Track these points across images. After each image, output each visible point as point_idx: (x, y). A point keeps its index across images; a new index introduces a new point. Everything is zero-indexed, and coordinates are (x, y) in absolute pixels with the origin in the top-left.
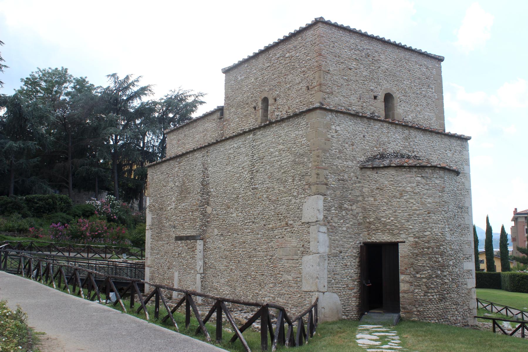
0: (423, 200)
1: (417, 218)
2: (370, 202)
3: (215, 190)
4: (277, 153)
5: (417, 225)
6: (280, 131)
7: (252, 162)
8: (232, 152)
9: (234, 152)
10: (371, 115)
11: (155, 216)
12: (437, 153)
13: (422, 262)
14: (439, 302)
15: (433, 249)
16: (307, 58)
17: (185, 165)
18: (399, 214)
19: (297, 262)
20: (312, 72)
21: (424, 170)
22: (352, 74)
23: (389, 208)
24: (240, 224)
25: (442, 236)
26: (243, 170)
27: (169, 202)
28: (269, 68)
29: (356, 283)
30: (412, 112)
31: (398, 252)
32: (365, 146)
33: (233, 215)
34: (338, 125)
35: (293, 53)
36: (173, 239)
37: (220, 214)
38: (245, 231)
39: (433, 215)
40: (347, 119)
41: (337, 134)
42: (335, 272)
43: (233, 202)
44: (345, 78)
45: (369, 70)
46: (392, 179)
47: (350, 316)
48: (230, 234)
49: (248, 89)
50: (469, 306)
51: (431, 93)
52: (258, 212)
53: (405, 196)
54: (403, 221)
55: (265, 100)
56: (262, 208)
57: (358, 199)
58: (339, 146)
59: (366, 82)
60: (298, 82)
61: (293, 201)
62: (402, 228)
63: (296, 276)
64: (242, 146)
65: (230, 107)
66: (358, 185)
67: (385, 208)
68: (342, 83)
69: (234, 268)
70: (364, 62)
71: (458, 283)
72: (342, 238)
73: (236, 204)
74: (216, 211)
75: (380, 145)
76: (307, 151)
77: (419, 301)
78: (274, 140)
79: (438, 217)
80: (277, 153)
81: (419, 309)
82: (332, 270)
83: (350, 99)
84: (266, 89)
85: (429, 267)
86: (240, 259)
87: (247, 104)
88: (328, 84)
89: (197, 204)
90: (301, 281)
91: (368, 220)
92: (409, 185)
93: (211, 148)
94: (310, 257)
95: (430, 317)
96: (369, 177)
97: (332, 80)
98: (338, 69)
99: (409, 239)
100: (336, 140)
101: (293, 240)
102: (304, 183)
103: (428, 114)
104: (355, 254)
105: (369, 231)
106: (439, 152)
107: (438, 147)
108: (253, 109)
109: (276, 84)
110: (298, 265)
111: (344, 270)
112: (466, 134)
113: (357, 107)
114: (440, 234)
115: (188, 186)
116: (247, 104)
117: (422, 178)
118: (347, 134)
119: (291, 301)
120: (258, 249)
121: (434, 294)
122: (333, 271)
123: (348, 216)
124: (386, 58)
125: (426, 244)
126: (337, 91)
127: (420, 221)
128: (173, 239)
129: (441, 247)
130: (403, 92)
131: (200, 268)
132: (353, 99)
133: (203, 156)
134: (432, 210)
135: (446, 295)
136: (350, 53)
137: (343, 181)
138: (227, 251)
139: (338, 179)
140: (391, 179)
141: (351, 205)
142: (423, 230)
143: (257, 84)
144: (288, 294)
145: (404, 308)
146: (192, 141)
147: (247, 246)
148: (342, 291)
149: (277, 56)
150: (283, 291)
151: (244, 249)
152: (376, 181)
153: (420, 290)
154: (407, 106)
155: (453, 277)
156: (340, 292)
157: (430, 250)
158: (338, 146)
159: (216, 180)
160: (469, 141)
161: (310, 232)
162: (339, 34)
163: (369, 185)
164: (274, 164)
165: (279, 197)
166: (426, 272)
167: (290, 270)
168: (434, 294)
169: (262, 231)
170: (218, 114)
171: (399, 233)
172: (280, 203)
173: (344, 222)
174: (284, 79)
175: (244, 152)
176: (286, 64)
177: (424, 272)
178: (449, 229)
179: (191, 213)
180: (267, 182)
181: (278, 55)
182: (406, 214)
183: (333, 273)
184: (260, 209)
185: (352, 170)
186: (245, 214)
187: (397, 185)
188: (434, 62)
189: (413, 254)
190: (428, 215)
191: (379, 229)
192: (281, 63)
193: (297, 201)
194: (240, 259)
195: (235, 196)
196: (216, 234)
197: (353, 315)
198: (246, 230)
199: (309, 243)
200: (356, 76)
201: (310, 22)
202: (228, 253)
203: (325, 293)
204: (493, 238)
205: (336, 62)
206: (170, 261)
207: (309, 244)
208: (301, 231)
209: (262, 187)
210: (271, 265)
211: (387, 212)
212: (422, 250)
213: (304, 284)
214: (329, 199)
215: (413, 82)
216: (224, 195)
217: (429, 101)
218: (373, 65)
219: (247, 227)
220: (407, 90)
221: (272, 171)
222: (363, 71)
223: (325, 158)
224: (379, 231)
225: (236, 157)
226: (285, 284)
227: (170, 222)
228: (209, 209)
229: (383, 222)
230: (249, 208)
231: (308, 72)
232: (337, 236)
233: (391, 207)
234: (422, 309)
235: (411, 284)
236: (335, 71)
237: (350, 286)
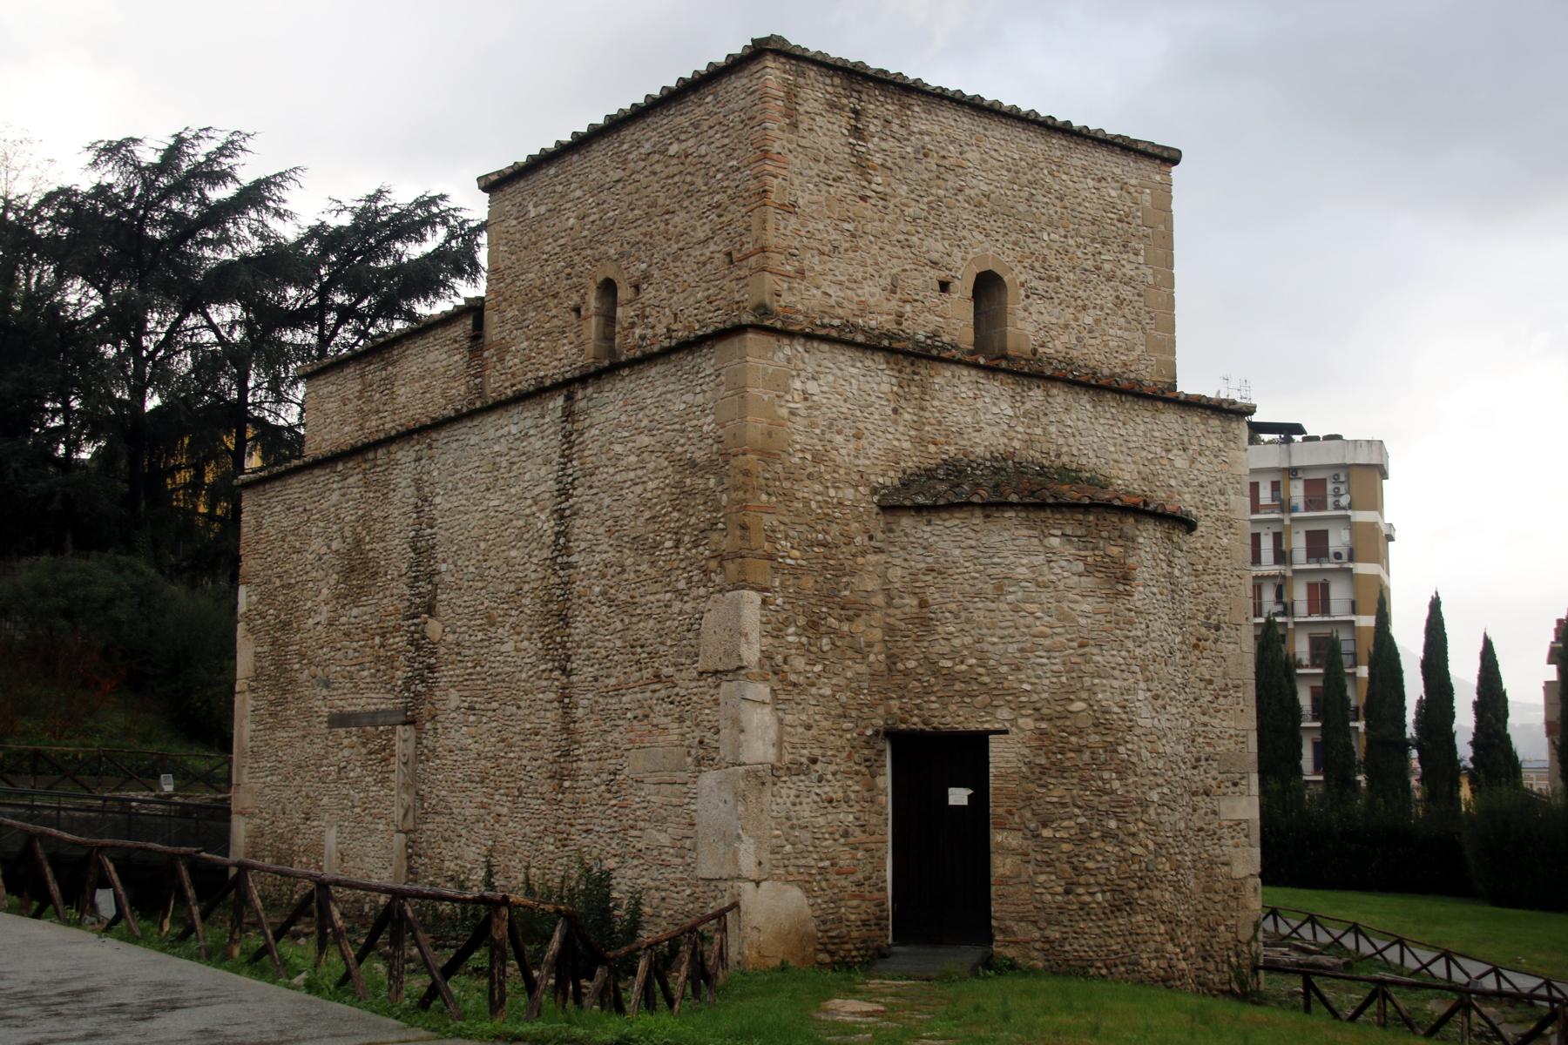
0: (1065, 605)
1: (1045, 661)
2: (907, 609)
3: (452, 567)
5: (1046, 682)
7: (561, 482)
8: (505, 450)
9: (510, 449)
10: (929, 341)
11: (266, 648)
12: (1138, 458)
13: (1059, 791)
14: (1112, 912)
15: (1093, 753)
16: (731, 164)
18: (991, 648)
20: (744, 210)
22: (868, 213)
23: (962, 630)
24: (524, 676)
25: (1124, 716)
27: (309, 604)
28: (621, 185)
31: (988, 763)
32: (899, 440)
33: (504, 648)
34: (813, 378)
35: (691, 142)
36: (321, 723)
37: (468, 644)
38: (541, 696)
39: (1095, 651)
40: (843, 357)
41: (808, 404)
42: (795, 821)
43: (505, 606)
45: (926, 200)
46: (973, 543)
47: (842, 953)
48: (495, 705)
49: (558, 249)
50: (1236, 933)
54: (1004, 669)
55: (608, 288)
57: (873, 601)
58: (816, 441)
59: (915, 239)
60: (701, 236)
61: (677, 606)
62: (998, 692)
64: (532, 432)
66: (872, 558)
67: (952, 629)
68: (836, 244)
69: (505, 811)
71: (1179, 857)
72: (817, 717)
73: (513, 613)
74: (454, 633)
75: (948, 436)
77: (1049, 911)
78: (624, 418)
79: (1113, 656)
80: (633, 458)
81: (1048, 932)
82: (783, 814)
83: (859, 291)
84: (612, 251)
85: (1080, 807)
86: (523, 784)
87: (555, 296)
89: (397, 610)
90: (694, 849)
92: (1024, 561)
93: (443, 434)
96: (906, 535)
97: (803, 233)
98: (822, 199)
99: (1021, 721)
100: (806, 422)
102: (707, 553)
105: (903, 697)
106: (1144, 454)
108: (573, 314)
109: (641, 237)
110: (687, 800)
113: (885, 317)
114: (1116, 709)
115: (371, 554)
117: (1065, 539)
118: (842, 403)
119: (667, 909)
120: (576, 752)
121: (1096, 889)
122: (788, 819)
124: (985, 161)
125: (1073, 739)
126: (818, 268)
127: (1055, 668)
128: (321, 723)
129: (1121, 749)
130: (1037, 265)
132: (871, 292)
133: (418, 459)
134: (1094, 635)
135: (1137, 894)
137: (824, 546)
138: (486, 758)
144: (657, 889)
145: (1003, 931)
147: (545, 741)
148: (818, 878)
149: (643, 151)
150: (644, 880)
151: (535, 754)
152: (925, 548)
154: (1050, 309)
155: (1159, 840)
157: (1086, 756)
158: (810, 441)
159: (455, 536)
161: (721, 700)
162: (829, 89)
163: (906, 560)
165: (636, 593)
166: (1072, 823)
167: (665, 814)
168: (1096, 889)
169: (590, 696)
170: (467, 325)
171: (990, 705)
172: (639, 611)
173: (824, 671)
174: (662, 226)
175: (539, 452)
176: (668, 177)
177: (1066, 823)
178: (1149, 694)
179: (377, 640)
180: (604, 547)
181: (647, 147)
182: (1012, 648)
183: (789, 823)
187: (988, 561)
188: (1148, 168)
189: (1031, 768)
190: (1081, 651)
191: (933, 692)
192: (655, 173)
193: (688, 607)
195: (512, 588)
196: (453, 705)
197: (850, 951)
198: (544, 692)
200: (881, 221)
201: (738, 50)
202: (489, 765)
203: (764, 885)
204: (1510, 720)
205: (817, 179)
206: (312, 794)
207: (716, 737)
208: (695, 698)
209: (588, 560)
210: (613, 802)
214: (779, 601)
215: (1073, 233)
216: (480, 585)
217: (1127, 292)
218: (940, 182)
219: (544, 683)
220: (1051, 259)
221: (618, 513)
223: (767, 479)
224: (933, 698)
225: (515, 467)
226: (649, 859)
227: (313, 668)
228: (434, 628)
229: (944, 672)
230: (552, 627)
231: (733, 207)
233: (967, 627)
234: (1058, 935)
235: (1025, 858)
236: (814, 207)
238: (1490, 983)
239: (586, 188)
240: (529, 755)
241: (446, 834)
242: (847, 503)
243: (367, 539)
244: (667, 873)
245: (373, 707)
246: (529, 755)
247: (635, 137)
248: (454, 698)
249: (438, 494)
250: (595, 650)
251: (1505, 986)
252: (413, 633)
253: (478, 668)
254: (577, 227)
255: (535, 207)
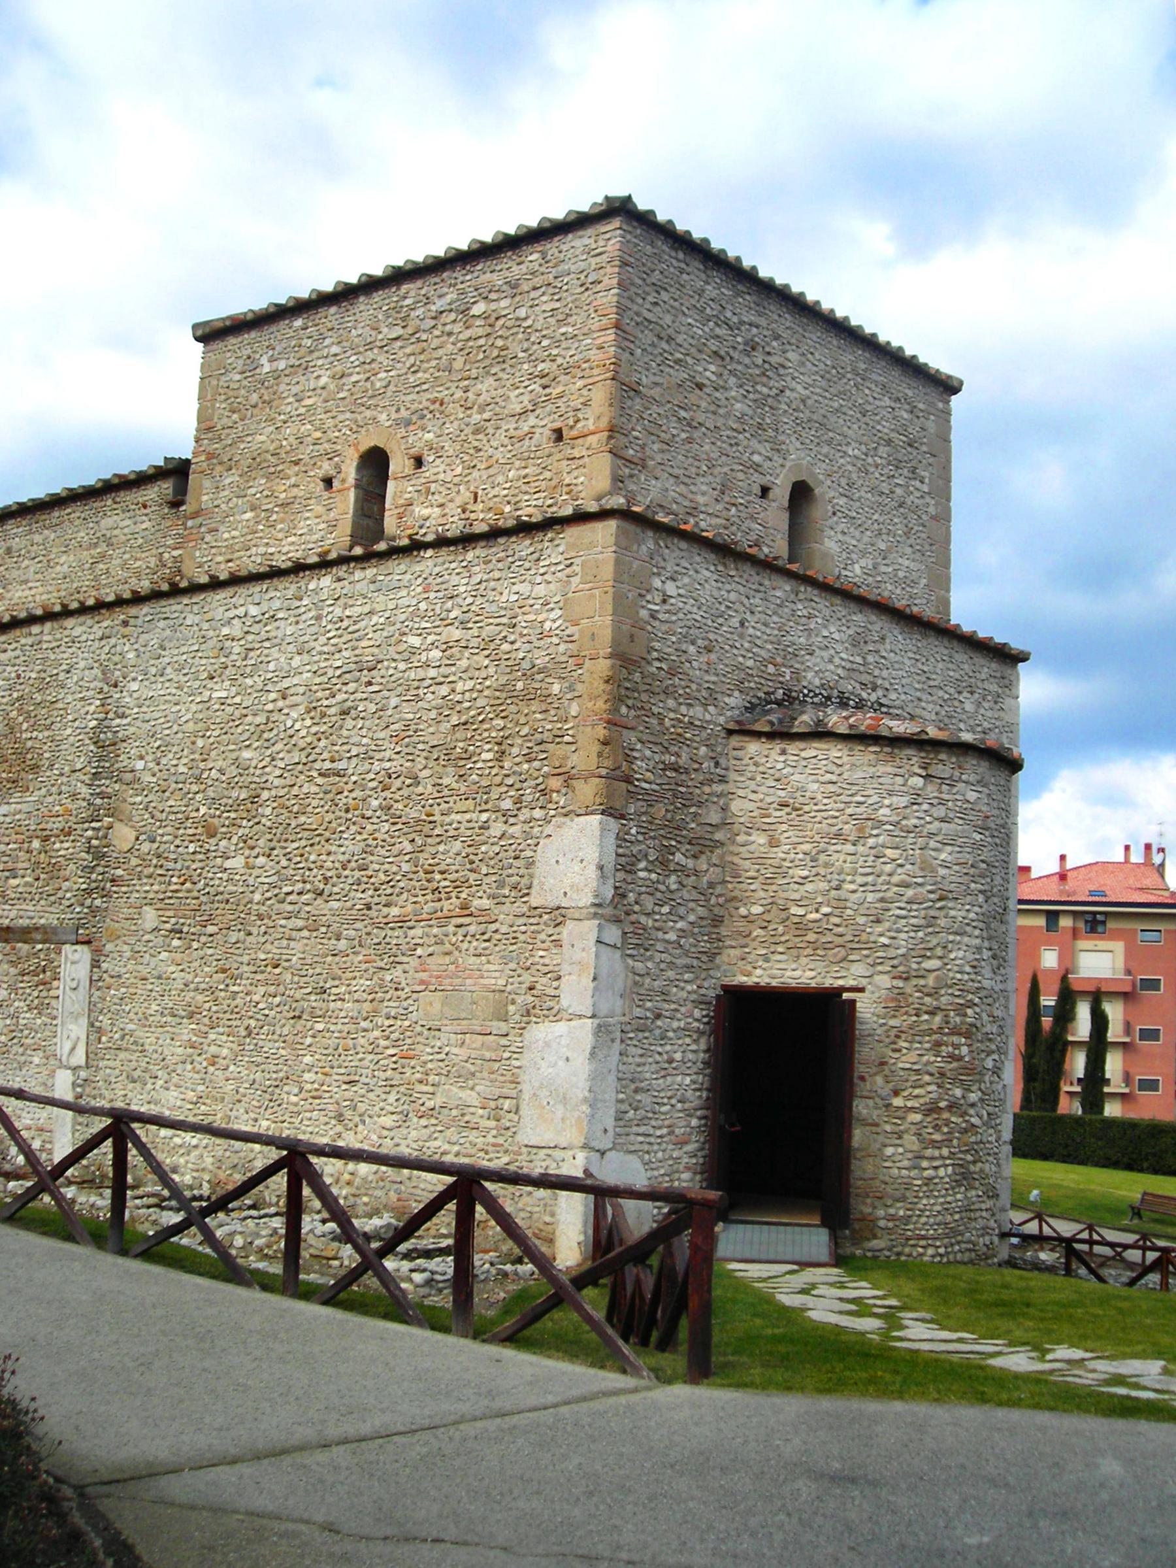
3: (151, 765)
4: (436, 654)
6: (454, 577)
9: (247, 633)
13: (912, 1057)
16: (563, 330)
17: (18, 661)
19: (504, 1041)
20: (580, 383)
21: (938, 752)
24: (257, 897)
26: (280, 704)
28: (399, 344)
29: (694, 1122)
30: (863, 554)
32: (744, 657)
33: (228, 864)
35: (504, 303)
37: (173, 856)
38: (283, 922)
43: (233, 815)
44: (683, 414)
46: (834, 778)
48: (211, 929)
49: (302, 410)
51: (918, 494)
52: (341, 858)
53: (871, 836)
54: (861, 920)
56: (362, 844)
59: (741, 436)
60: (518, 409)
61: (497, 829)
63: (497, 1092)
65: (219, 468)
70: (740, 368)
73: (245, 822)
76: (564, 659)
78: (423, 606)
80: (436, 654)
83: (692, 487)
86: (253, 1023)
87: (296, 463)
88: (633, 429)
91: (743, 911)
92: (887, 802)
94: (561, 1028)
95: (924, 1238)
96: (756, 764)
101: (492, 967)
103: (907, 563)
104: (696, 1024)
106: (941, 693)
107: (939, 678)
109: (425, 404)
110: (507, 1055)
111: (664, 1077)
112: (1016, 644)
116: (296, 463)
118: (695, 610)
123: (685, 894)
125: (927, 1000)
131: (73, 1049)
135: (972, 1168)
136: (700, 332)
137: (676, 770)
139: (663, 763)
140: (829, 777)
141: (695, 857)
142: (923, 953)
143: (341, 395)
146: (39, 576)
147: (288, 977)
148: (656, 1147)
149: (433, 308)
150: (437, 1143)
151: (272, 989)
153: (901, 1150)
154: (852, 530)
156: (648, 1152)
157: (938, 1019)
160: (1020, 664)
161: (564, 943)
162: (674, 262)
164: (421, 692)
167: (472, 1069)
169: (359, 925)
172: (436, 832)
174: (459, 394)
179: (36, 844)
180: (388, 754)
181: (440, 304)
182: (870, 897)
183: (633, 1086)
184: (351, 847)
185: (704, 735)
186: (284, 863)
187: (848, 799)
188: (933, 394)
190: (939, 905)
194: (253, 1023)
196: (149, 926)
199: (559, 978)
202: (200, 998)
203: (608, 1153)
207: (555, 984)
208: (522, 937)
210: (391, 1051)
211: (809, 887)
212: (914, 1018)
213: (526, 1121)
215: (872, 453)
216: (195, 788)
218: (764, 379)
219: (290, 908)
222: (734, 398)
223: (627, 689)
224: (780, 949)
225: (251, 654)
229: (796, 920)
230: (303, 843)
232: (651, 958)
234: (901, 1213)
237: (677, 1131)
238: (1032, 1228)
239: (345, 344)
240: (262, 990)
241: (136, 1074)
242: (697, 723)
243: (25, 726)
244: (473, 1135)
245: (28, 921)
246: (262, 990)
247: (423, 292)
248: (150, 917)
249: (134, 679)
250: (370, 873)
251: (1047, 1231)
252: (89, 840)
253: (188, 885)
254: (332, 387)
255: (272, 360)
